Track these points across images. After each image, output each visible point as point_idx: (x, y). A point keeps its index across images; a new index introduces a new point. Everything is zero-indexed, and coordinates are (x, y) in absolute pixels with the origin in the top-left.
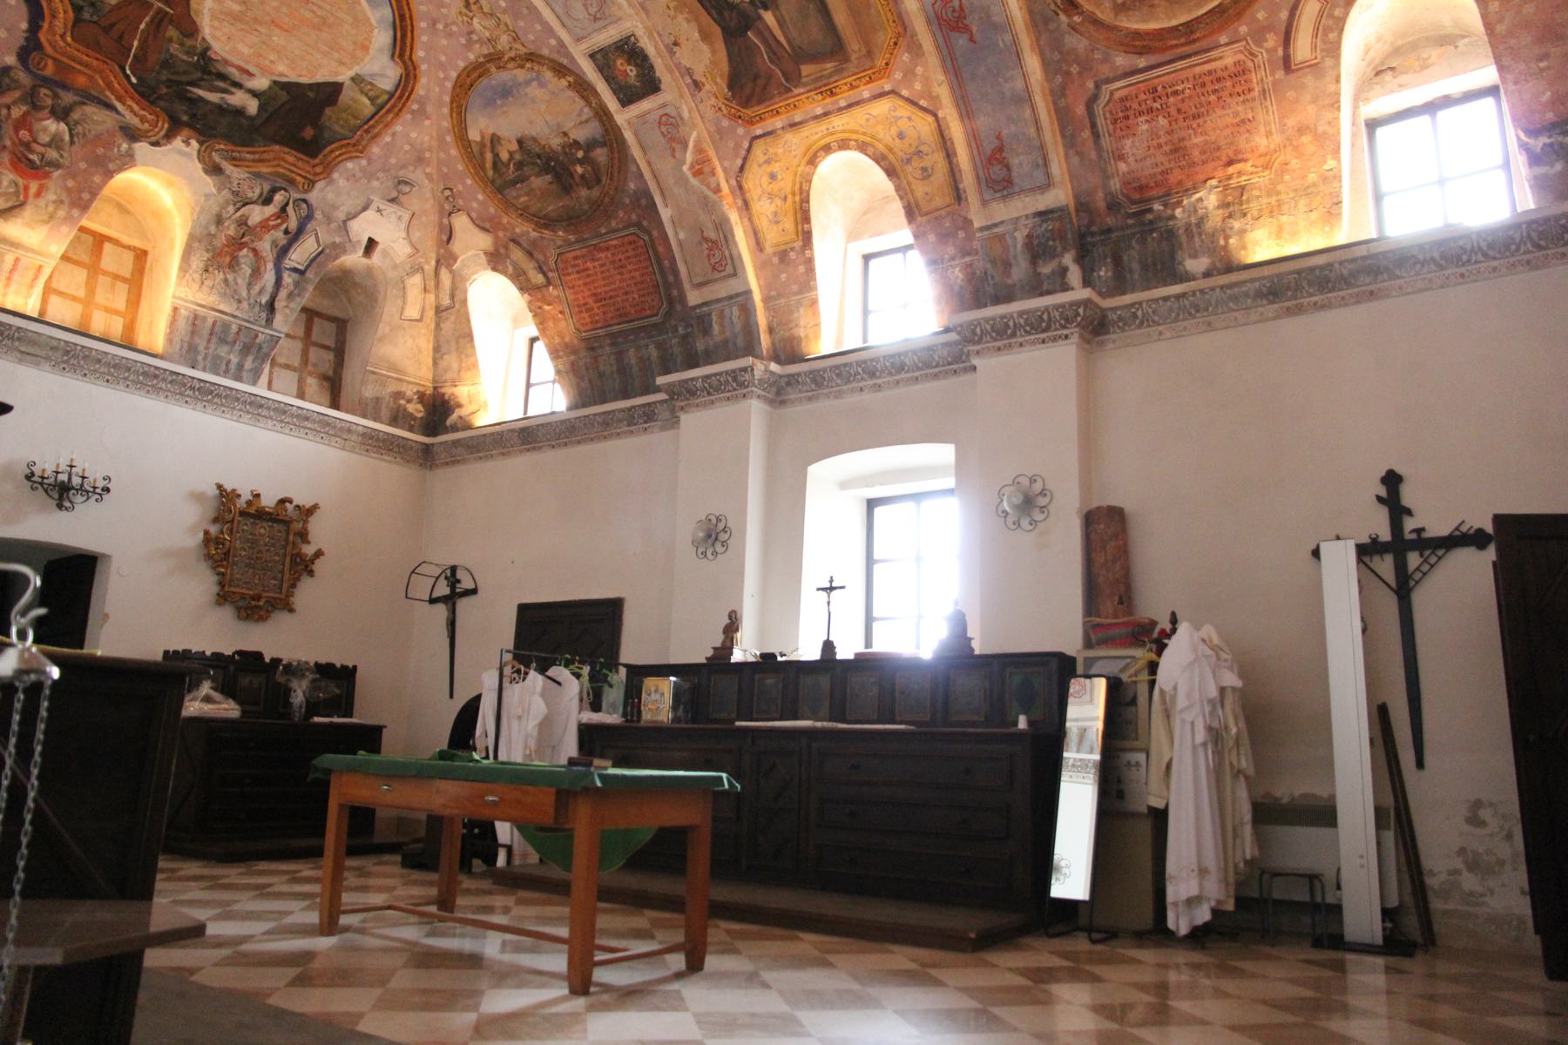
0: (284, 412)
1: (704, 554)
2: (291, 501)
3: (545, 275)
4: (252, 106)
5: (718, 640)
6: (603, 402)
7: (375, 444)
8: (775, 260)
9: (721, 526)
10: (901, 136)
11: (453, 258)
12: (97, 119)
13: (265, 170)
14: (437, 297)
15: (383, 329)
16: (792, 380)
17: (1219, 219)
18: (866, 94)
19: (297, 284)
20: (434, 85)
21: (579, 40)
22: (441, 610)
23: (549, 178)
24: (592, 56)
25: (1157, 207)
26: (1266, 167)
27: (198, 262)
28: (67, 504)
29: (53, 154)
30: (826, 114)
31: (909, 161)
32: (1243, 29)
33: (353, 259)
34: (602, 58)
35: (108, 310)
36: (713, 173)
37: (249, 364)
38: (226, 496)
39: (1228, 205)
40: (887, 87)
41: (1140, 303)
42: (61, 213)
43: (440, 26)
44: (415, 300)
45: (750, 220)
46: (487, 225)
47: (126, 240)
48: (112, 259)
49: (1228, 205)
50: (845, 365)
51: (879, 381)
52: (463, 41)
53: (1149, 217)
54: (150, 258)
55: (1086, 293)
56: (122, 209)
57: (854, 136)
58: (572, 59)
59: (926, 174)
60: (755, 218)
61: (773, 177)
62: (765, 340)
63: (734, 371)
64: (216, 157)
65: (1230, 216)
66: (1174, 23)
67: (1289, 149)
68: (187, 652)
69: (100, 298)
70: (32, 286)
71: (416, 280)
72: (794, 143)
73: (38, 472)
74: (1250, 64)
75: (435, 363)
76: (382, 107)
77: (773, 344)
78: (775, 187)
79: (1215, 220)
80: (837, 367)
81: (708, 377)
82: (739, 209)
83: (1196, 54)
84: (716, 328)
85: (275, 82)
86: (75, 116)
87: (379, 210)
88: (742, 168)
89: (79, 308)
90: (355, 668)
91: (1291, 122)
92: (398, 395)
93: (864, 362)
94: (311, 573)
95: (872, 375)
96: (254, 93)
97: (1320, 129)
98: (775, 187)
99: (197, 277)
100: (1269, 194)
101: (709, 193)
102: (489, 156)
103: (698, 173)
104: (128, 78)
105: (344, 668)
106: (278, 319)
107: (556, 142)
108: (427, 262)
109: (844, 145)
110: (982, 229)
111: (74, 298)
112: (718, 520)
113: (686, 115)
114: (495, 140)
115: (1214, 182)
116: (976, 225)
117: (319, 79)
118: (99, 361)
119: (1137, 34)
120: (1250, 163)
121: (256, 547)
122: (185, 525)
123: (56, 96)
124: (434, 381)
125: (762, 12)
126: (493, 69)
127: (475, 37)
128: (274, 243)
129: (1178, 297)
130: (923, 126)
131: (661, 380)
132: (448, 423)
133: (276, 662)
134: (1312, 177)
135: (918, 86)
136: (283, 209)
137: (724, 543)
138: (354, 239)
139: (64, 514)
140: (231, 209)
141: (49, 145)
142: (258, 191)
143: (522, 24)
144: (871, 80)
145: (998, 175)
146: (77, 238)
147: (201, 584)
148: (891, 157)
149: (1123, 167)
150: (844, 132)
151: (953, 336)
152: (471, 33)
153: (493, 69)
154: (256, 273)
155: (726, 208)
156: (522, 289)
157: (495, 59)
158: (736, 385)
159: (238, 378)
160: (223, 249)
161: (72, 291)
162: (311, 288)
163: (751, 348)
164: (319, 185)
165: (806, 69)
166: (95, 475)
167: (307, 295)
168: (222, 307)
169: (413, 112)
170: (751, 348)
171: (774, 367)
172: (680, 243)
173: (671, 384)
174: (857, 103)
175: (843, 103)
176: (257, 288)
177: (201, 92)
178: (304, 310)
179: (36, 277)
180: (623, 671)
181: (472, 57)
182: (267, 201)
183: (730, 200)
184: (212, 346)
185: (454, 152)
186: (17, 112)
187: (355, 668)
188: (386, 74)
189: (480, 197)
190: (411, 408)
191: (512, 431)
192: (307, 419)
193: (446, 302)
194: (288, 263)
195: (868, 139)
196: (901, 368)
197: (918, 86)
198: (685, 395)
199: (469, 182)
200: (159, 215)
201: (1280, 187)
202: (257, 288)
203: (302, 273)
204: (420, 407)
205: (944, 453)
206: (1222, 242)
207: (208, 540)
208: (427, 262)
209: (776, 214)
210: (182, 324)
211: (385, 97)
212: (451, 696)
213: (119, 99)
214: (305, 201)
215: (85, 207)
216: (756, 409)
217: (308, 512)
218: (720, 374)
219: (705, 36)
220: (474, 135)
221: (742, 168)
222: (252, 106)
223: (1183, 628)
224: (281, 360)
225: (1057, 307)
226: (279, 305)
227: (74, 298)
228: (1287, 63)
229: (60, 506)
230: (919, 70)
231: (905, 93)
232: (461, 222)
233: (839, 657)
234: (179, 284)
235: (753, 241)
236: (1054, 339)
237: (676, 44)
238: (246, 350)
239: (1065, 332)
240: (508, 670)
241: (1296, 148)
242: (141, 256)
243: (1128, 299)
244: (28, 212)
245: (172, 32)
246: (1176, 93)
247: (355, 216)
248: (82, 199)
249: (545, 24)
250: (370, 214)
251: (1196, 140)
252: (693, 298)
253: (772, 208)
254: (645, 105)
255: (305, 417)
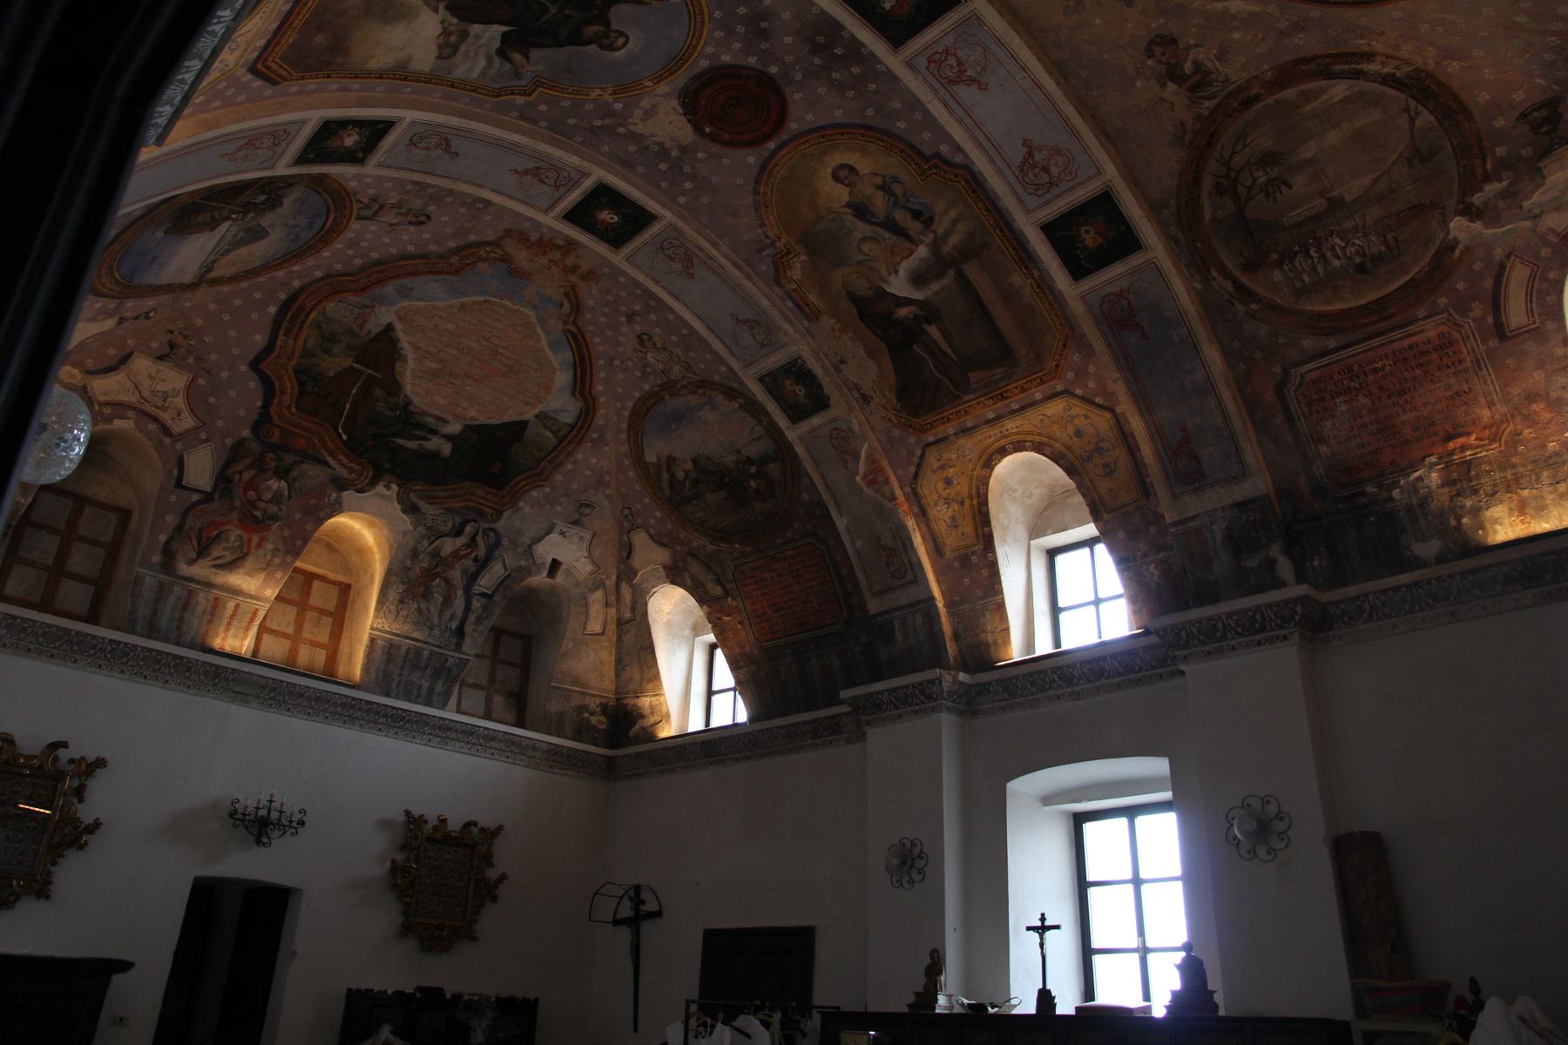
0: (472, 734)
1: (900, 882)
2: (475, 824)
3: (724, 587)
4: (446, 449)
5: (920, 983)
6: (787, 713)
7: (556, 758)
8: (957, 564)
9: (916, 851)
10: (1078, 433)
11: (633, 572)
12: (313, 474)
13: (457, 504)
14: (618, 610)
15: (567, 644)
16: (982, 689)
17: (1446, 498)
18: (1038, 396)
19: (485, 608)
20: (612, 414)
21: (748, 366)
22: (625, 933)
23: (723, 493)
24: (761, 379)
25: (1370, 489)
26: (1494, 439)
27: (393, 595)
28: (265, 840)
29: (274, 509)
30: (998, 418)
31: (1089, 458)
32: (1443, 301)
33: (539, 579)
34: (771, 381)
35: (314, 644)
36: (887, 482)
37: (439, 688)
38: (413, 822)
39: (1454, 482)
40: (1060, 388)
41: (1366, 596)
42: (277, 561)
43: (617, 363)
44: (597, 616)
45: (928, 525)
46: (665, 540)
47: (331, 576)
48: (321, 596)
49: (1454, 482)
50: (1039, 672)
51: (1077, 689)
52: (638, 373)
53: (1363, 500)
54: (352, 591)
55: (1303, 590)
56: (331, 548)
57: (1029, 438)
58: (742, 383)
59: (1109, 470)
60: (933, 524)
61: (948, 482)
62: (951, 647)
63: (921, 684)
64: (413, 497)
65: (1458, 494)
66: (1363, 301)
67: (1518, 419)
68: (369, 991)
69: (306, 634)
70: (248, 629)
71: (598, 595)
72: (969, 447)
73: (240, 810)
74: (1458, 336)
75: (617, 675)
76: (564, 439)
77: (960, 650)
78: (950, 492)
79: (1442, 498)
80: (1031, 674)
81: (894, 690)
82: (915, 516)
83: (1392, 330)
84: (899, 636)
85: (467, 426)
86: (294, 474)
87: (562, 533)
88: (916, 475)
89: (287, 643)
90: (537, 1000)
91: (1515, 391)
92: (582, 708)
93: (1060, 668)
94: (494, 899)
95: (1070, 681)
96: (448, 437)
97: (1554, 395)
98: (950, 492)
99: (393, 608)
100: (1502, 468)
101: (885, 502)
102: (665, 476)
103: (871, 483)
104: (339, 435)
105: (526, 1001)
106: (468, 641)
107: (729, 459)
108: (608, 578)
109: (1019, 447)
110: (1176, 524)
111: (285, 635)
112: (913, 845)
113: (856, 428)
114: (671, 460)
115: (1433, 459)
116: (1169, 519)
117: (507, 418)
118: (302, 695)
119: (1322, 316)
120: (1474, 437)
121: (440, 872)
122: (371, 854)
123: (280, 459)
124: (617, 692)
125: (926, 326)
126: (667, 397)
127: (649, 370)
128: (465, 571)
129: (1409, 586)
130: (1101, 422)
131: (845, 694)
132: (631, 733)
133: (457, 997)
134: (1552, 446)
135: (1092, 384)
136: (473, 539)
137: (921, 871)
138: (539, 561)
139: (263, 851)
140: (425, 543)
141: (270, 501)
142: (450, 524)
143: (692, 355)
144: (1042, 382)
145: (1187, 469)
146: (291, 578)
147: (385, 916)
148: (1069, 455)
149: (1324, 450)
150: (1017, 434)
151: (1153, 639)
152: (645, 366)
153: (667, 397)
154: (448, 601)
155: (902, 515)
156: (700, 601)
157: (670, 387)
158: (924, 700)
159: (428, 703)
160: (413, 580)
161: (282, 629)
162: (498, 611)
163: (936, 658)
164: (506, 515)
165: (974, 377)
166: (292, 807)
167: (495, 617)
168: (415, 635)
169: (593, 441)
170: (936, 658)
171: (962, 676)
172: (857, 551)
173: (856, 698)
174: (1030, 405)
175: (1015, 406)
176: (448, 614)
177: (401, 442)
178: (493, 629)
179: (252, 620)
180: (817, 1017)
181: (646, 387)
182: (458, 532)
183: (905, 507)
184: (405, 672)
185: (631, 474)
186: (247, 476)
187: (537, 1000)
188: (563, 405)
189: (658, 514)
190: (594, 720)
191: (694, 744)
192: (493, 739)
193: (628, 615)
194: (477, 589)
195: (1044, 439)
196: (1100, 674)
197: (1092, 384)
198: (869, 710)
199: (647, 500)
200: (362, 551)
201: (1514, 460)
202: (448, 614)
203: (490, 597)
204: (602, 718)
205: (1159, 766)
206: (1453, 523)
207: (395, 868)
208: (608, 578)
209: (953, 518)
210: (378, 653)
211: (567, 429)
212: (636, 1029)
213: (332, 454)
214: (492, 530)
215: (296, 553)
216: (946, 724)
217: (492, 834)
218: (907, 686)
219: (871, 353)
220: (651, 457)
221: (916, 475)
222: (446, 449)
223: (1493, 1005)
224: (471, 680)
225: (1270, 606)
226: (468, 629)
227: (285, 635)
228: (1500, 331)
229: (258, 842)
230: (1091, 369)
231: (1078, 392)
232: (640, 539)
233: (1058, 1012)
234: (376, 616)
235: (932, 545)
236: (1271, 641)
237: (842, 362)
238: (436, 675)
239: (1283, 632)
240: (693, 1022)
241: (1526, 417)
242: (345, 589)
243: (1351, 591)
244: (249, 563)
245: (379, 393)
246: (1375, 371)
247: (540, 540)
248: (295, 546)
249: (716, 354)
250: (554, 537)
251: (1404, 418)
252: (874, 606)
253: (950, 513)
254: (816, 421)
255: (491, 737)
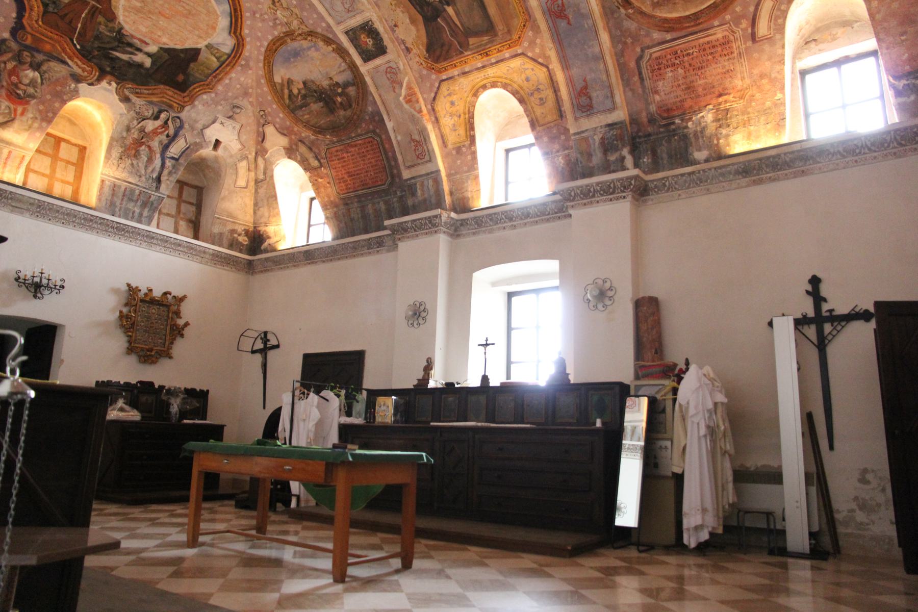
0: (167, 242)
1: (412, 324)
2: (170, 294)
3: (319, 161)
4: (148, 62)
5: (420, 375)
6: (353, 235)
7: (220, 260)
8: (454, 152)
9: (422, 308)
10: (527, 80)
11: (265, 151)
12: (57, 70)
13: (155, 99)
14: (256, 174)
15: (224, 192)
16: (464, 223)
17: (714, 128)
18: (507, 55)
19: (174, 166)
20: (254, 50)
21: (339, 23)
22: (258, 357)
23: (321, 104)
24: (347, 33)
25: (677, 121)
26: (741, 98)
27: (116, 153)
28: (39, 295)
29: (31, 90)
30: (483, 67)
31: (532, 94)
32: (728, 17)
33: (207, 152)
34: (353, 34)
35: (64, 182)
36: (418, 101)
37: (146, 213)
38: (132, 291)
39: (719, 120)
40: (520, 51)
41: (668, 178)
42: (36, 125)
43: (257, 15)
44: (243, 176)
45: (439, 129)
46: (285, 132)
47: (74, 140)
48: (66, 152)
49: (719, 120)
50: (495, 214)
51: (514, 223)
52: (271, 24)
53: (673, 127)
54: (88, 151)
55: (636, 172)
56: (72, 122)
57: (500, 80)
58: (335, 35)
59: (542, 102)
60: (442, 128)
61: (452, 103)
62: (448, 199)
63: (430, 217)
64: (127, 92)
65: (720, 127)
66: (687, 13)
67: (755, 87)
68: (109, 382)
69: (59, 174)
70: (18, 167)
71: (244, 164)
72: (465, 84)
73: (22, 276)
74: (732, 38)
75: (255, 213)
76: (224, 63)
77: (453, 201)
78: (454, 109)
79: (711, 129)
80: (490, 215)
81: (414, 221)
82: (433, 123)
83: (700, 31)
84: (419, 192)
85: (161, 48)
86: (44, 68)
87: (222, 123)
88: (434, 99)
89: (46, 180)
90: (208, 391)
91: (756, 71)
92: (233, 231)
93: (506, 212)
94: (182, 336)
95: (511, 219)
96: (149, 55)
97: (773, 76)
98: (454, 109)
99: (115, 162)
100: (743, 114)
101: (415, 113)
102: (286, 91)
103: (409, 101)
104: (75, 45)
105: (201, 391)
106: (163, 187)
107: (325, 83)
108: (250, 154)
109: (494, 85)
110: (575, 134)
111: (43, 175)
112: (421, 304)
113: (401, 67)
114: (290, 82)
115: (711, 107)
116: (572, 132)
117: (187, 46)
118: (58, 211)
119: (666, 20)
120: (732, 96)
121: (150, 321)
122: (108, 307)
123: (33, 56)
124: (254, 223)
125: (446, 7)
126: (289, 41)
127: (278, 22)
128: (161, 142)
129: (690, 174)
130: (540, 74)
131: (387, 223)
132: (262, 248)
133: (162, 388)
134: (768, 104)
135: (537, 50)
136: (166, 123)
137: (424, 318)
138: (207, 140)
139: (37, 301)
140: (135, 122)
141: (29, 85)
142: (151, 112)
143: (305, 14)
144: (510, 47)
145: (584, 103)
146: (45, 139)
147: (118, 342)
148: (522, 92)
149: (657, 98)
150: (494, 77)
151: (558, 197)
152: (276, 19)
153: (289, 41)
154: (150, 160)
155: (425, 122)
156: (305, 169)
157: (290, 34)
158: (431, 226)
159: (139, 222)
160: (130, 146)
161: (42, 171)
162: (182, 169)
163: (439, 204)
164: (187, 109)
165: (472, 41)
166: (56, 278)
167: (180, 173)
168: (130, 180)
169: (242, 66)
170: (439, 204)
171: (453, 215)
172: (398, 142)
173: (393, 225)
174: (502, 60)
175: (493, 61)
176: (150, 169)
177: (118, 54)
178: (178, 181)
179: (21, 162)
180: (365, 393)
181: (276, 33)
182: (156, 118)
183: (427, 117)
184: (124, 203)
185: (266, 89)
186: (10, 66)
187: (208, 391)
188: (226, 43)
189: (281, 115)
190: (241, 239)
191: (300, 252)
192: (180, 245)
193: (261, 177)
194: (168, 154)
195: (508, 82)
196: (528, 216)
197: (537, 50)
198: (401, 231)
199: (275, 106)
200: (93, 126)
201: (749, 110)
202: (150, 169)
203: (177, 160)
204: (246, 238)
205: (553, 265)
206: (715, 142)
207: (122, 316)
208: (250, 154)
209: (454, 125)
210: (107, 190)
211: (226, 57)
212: (264, 408)
213: (70, 58)
214: (178, 118)
215: (50, 121)
216: (442, 240)
217: (180, 300)
218: (422, 219)
219: (413, 21)
220: (277, 79)
221: (434, 99)
222: (148, 62)
223: (693, 368)
224: (165, 211)
225: (619, 180)
226: (163, 178)
227: (43, 175)
228: (753, 37)
229: (35, 297)
230: (538, 41)
231: (530, 54)
232: (270, 130)
233: (491, 385)
234: (105, 166)
235: (441, 141)
236: (617, 199)
237: (396, 26)
238: (144, 205)
239: (624, 194)
240: (297, 393)
241: (759, 87)
242: (83, 150)
243: (660, 175)
244: (16, 124)
245: (101, 19)
246: (688, 54)
247: (208, 127)
248: (48, 116)
249: (319, 14)
250: (217, 125)
251: (700, 82)
252: (406, 174)
253: (452, 122)
254: (378, 61)
255: (179, 244)
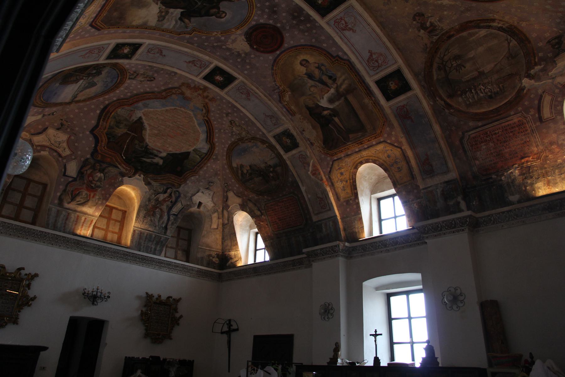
0: (170, 265)
1: (324, 318)
2: (171, 297)
3: (261, 212)
4: (161, 162)
5: (331, 355)
6: (284, 257)
7: (200, 273)
8: (345, 204)
9: (330, 307)
10: (389, 156)
11: (228, 206)
12: (113, 171)
13: (164, 182)
14: (223, 220)
15: (204, 232)
16: (354, 249)
17: (521, 179)
18: (374, 143)
19: (175, 219)
20: (220, 149)
21: (269, 132)
22: (225, 337)
23: (261, 178)
24: (274, 137)
25: (494, 176)
26: (538, 158)
27: (142, 215)
28: (95, 303)
29: (99, 184)
30: (360, 151)
31: (392, 165)
32: (520, 109)
33: (194, 209)
34: (278, 137)
35: (113, 232)
36: (320, 174)
37: (158, 248)
38: (149, 297)
39: (524, 174)
40: (382, 140)
41: (492, 215)
42: (100, 202)
43: (222, 131)
44: (215, 222)
45: (334, 190)
46: (240, 195)
47: (119, 208)
48: (116, 215)
49: (524, 174)
50: (374, 243)
51: (388, 248)
52: (230, 135)
53: (491, 180)
54: (127, 213)
55: (469, 213)
56: (119, 198)
57: (371, 158)
58: (267, 138)
59: (400, 170)
60: (336, 189)
61: (342, 174)
62: (343, 234)
63: (332, 247)
64: (149, 179)
65: (525, 178)
66: (491, 109)
67: (547, 151)
68: (133, 358)
69: (110, 229)
70: (89, 227)
71: (216, 215)
72: (349, 161)
73: (87, 292)
74: (525, 121)
75: (222, 243)
76: (203, 158)
77: (346, 235)
78: (342, 177)
79: (519, 179)
80: (371, 243)
81: (322, 249)
82: (330, 186)
83: (502, 119)
84: (324, 230)
85: (168, 154)
86: (106, 171)
87: (203, 192)
88: (330, 171)
89: (103, 232)
90: (193, 361)
91: (546, 141)
92: (210, 255)
93: (382, 241)
94: (178, 324)
95: (385, 246)
96: (161, 158)
97: (560, 142)
98: (342, 177)
99: (142, 219)
100: (541, 169)
101: (319, 181)
102: (240, 172)
103: (314, 174)
104: (122, 157)
105: (190, 361)
106: (168, 231)
107: (263, 166)
108: (219, 208)
109: (367, 161)
110: (424, 189)
111: (103, 229)
112: (329, 305)
113: (308, 154)
114: (242, 166)
115: (516, 166)
116: (421, 187)
117: (183, 151)
118: (109, 251)
119: (476, 114)
120: (531, 158)
121: (158, 315)
122: (134, 308)
123: (101, 166)
124: (222, 250)
125: (333, 118)
126: (240, 143)
127: (234, 133)
128: (167, 206)
129: (508, 212)
130: (397, 152)
131: (304, 250)
132: (227, 265)
133: (165, 360)
134: (559, 161)
135: (393, 139)
136: (170, 195)
137: (332, 314)
138: (194, 203)
139: (95, 307)
140: (153, 196)
141: (97, 181)
142: (162, 189)
143: (249, 128)
144: (376, 138)
145: (428, 169)
146: (105, 209)
147: (139, 331)
148: (385, 164)
149: (477, 162)
150: (367, 156)
151: (416, 231)
152: (232, 132)
153: (240, 143)
154: (161, 217)
155: (325, 186)
156: (252, 217)
157: (241, 140)
158: (333, 252)
159: (154, 254)
161: (102, 227)
162: (179, 220)
163: (337, 237)
164: (182, 186)
165: (351, 136)
166: (105, 291)
167: (178, 223)
168: (150, 229)
169: (213, 159)
170: (337, 237)
171: (347, 244)
172: (309, 199)
173: (308, 252)
174: (371, 146)
175: (366, 147)
176: (161, 222)
177: (145, 159)
178: (178, 227)
179: (91, 224)
180: (294, 367)
181: (233, 140)
182: (165, 192)
183: (326, 183)
184: (146, 243)
185: (227, 171)
186: (89, 172)
187: (193, 361)
188: (203, 146)
189: (237, 186)
190: (214, 260)
191: (250, 268)
192: (178, 267)
193: (226, 222)
194: (172, 212)
195: (376, 159)
196: (396, 243)
197: (393, 139)
198: (313, 256)
199: (233, 181)
200: (130, 199)
201: (546, 166)
202: (161, 222)
203: (176, 215)
204: (217, 259)
205: (418, 276)
206: (524, 189)
207: (142, 313)
208: (219, 208)
209: (344, 187)
210: (136, 236)
211: (204, 155)
212: (229, 371)
213: (120, 164)
214: (177, 191)
215: (107, 199)
216: (341, 261)
217: (177, 301)
218: (327, 248)
219: (314, 127)
220: (234, 165)
221: (330, 171)
222: (161, 162)
223: (538, 363)
224: (170, 245)
225: (458, 219)
226: (169, 227)
227: (103, 229)
228: (541, 119)
229: (93, 304)
230: (393, 133)
231: (388, 141)
232: (231, 194)
233: (381, 365)
234: (135, 222)
235: (336, 197)
236: (458, 231)
237: (303, 131)
238: (157, 244)
239: (462, 228)
240: (250, 369)
241: (550, 151)
242: (124, 213)
243: (487, 213)
244: (90, 203)
245: (137, 142)
246: (495, 134)
247: (194, 195)
248: (106, 197)
249: (258, 128)
250: (200, 194)
251: (506, 151)
252: (315, 219)
253: (342, 185)
254: (294, 152)
255: (177, 266)
